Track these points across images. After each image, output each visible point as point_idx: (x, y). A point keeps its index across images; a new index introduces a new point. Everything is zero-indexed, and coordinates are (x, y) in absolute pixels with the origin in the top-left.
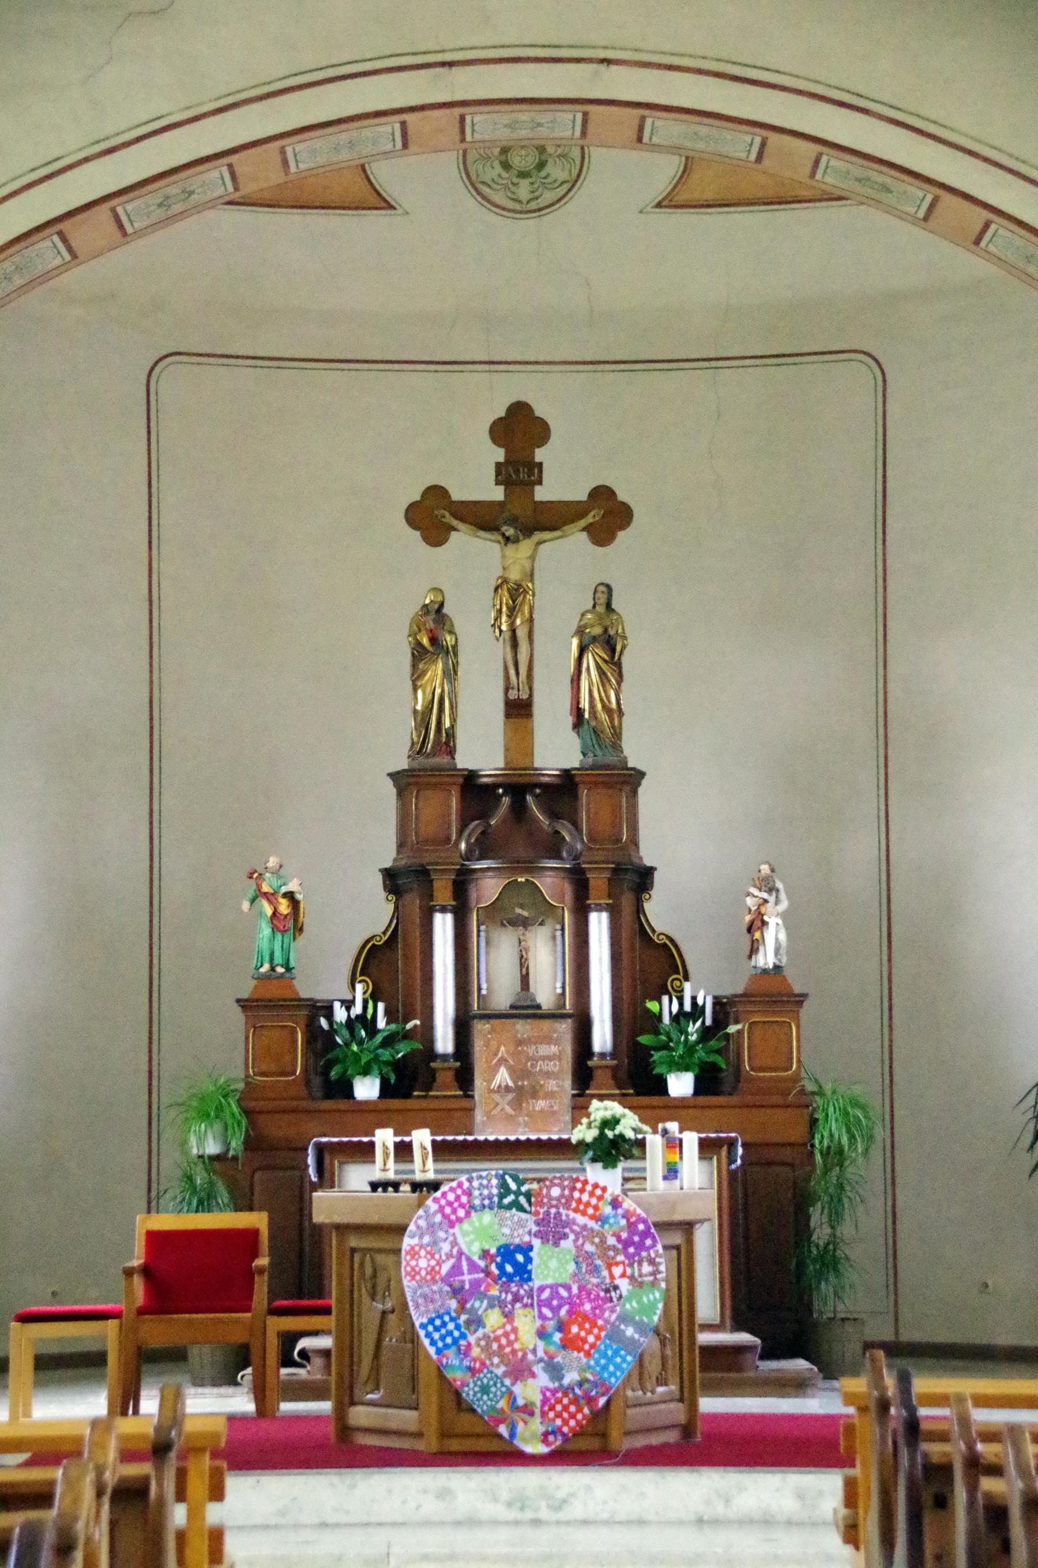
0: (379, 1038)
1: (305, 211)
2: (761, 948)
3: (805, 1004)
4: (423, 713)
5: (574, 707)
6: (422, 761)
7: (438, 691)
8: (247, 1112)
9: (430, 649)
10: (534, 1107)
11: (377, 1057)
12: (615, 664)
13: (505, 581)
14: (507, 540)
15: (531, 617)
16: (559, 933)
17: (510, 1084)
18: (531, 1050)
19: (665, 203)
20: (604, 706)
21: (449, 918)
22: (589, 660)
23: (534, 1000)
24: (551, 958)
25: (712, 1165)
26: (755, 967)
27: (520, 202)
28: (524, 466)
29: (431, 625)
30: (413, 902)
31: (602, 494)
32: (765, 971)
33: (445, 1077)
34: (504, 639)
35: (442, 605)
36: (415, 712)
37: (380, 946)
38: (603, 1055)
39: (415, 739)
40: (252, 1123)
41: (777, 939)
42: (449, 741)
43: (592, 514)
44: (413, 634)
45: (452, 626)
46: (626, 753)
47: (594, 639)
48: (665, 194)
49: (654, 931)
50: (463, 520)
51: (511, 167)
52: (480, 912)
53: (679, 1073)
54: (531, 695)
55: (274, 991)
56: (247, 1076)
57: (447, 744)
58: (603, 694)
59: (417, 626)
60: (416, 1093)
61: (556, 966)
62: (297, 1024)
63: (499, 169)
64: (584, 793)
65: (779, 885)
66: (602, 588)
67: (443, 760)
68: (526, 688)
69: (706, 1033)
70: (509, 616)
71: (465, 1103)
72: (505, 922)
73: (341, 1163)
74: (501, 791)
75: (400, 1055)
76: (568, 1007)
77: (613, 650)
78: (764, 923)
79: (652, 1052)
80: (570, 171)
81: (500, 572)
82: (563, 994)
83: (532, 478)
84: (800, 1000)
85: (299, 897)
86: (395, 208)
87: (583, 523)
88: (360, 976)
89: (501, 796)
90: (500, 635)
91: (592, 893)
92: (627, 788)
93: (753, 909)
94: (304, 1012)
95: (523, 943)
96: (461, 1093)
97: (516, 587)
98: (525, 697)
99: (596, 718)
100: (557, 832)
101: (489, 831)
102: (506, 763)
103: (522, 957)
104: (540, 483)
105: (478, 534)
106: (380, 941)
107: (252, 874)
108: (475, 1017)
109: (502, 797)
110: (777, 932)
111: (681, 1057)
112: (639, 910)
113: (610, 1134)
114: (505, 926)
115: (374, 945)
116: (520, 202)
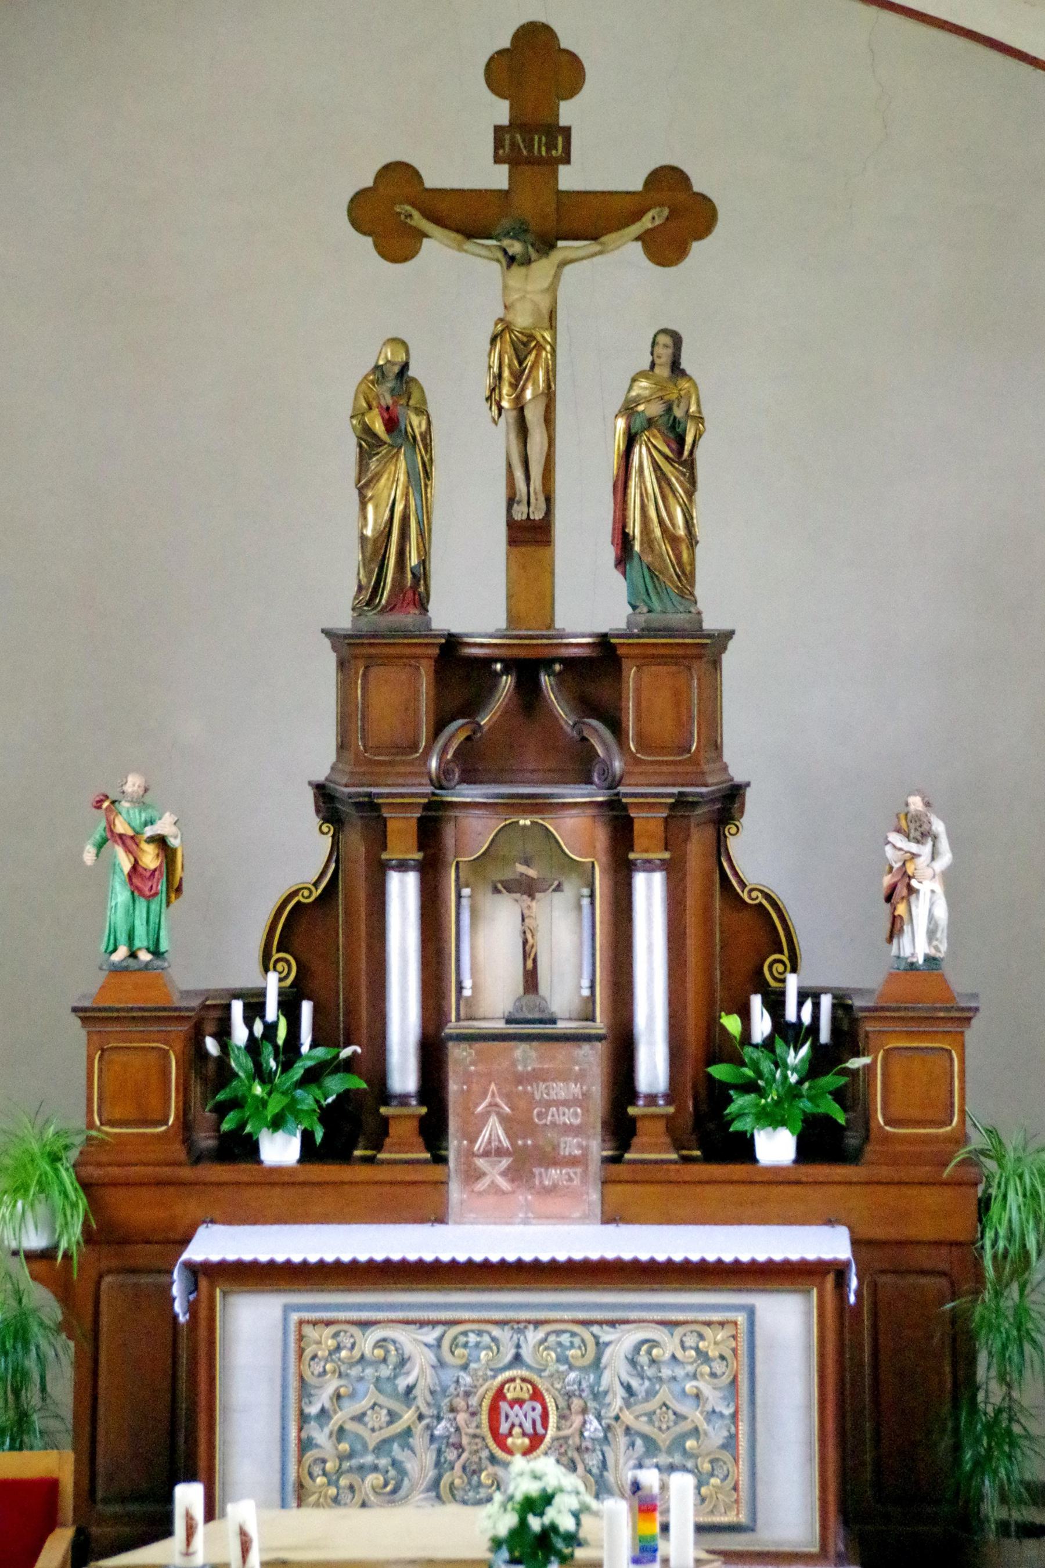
0: (298, 1072)
2: (907, 928)
3: (973, 1022)
4: (375, 540)
5: (619, 532)
6: (373, 619)
7: (399, 508)
8: (86, 1186)
11: (294, 1101)
12: (683, 463)
14: (511, 260)
15: (549, 387)
16: (586, 902)
17: (506, 1143)
18: (539, 1090)
21: (412, 879)
22: (640, 454)
25: (810, 1301)
30: (355, 841)
35: (405, 367)
36: (363, 538)
37: (309, 904)
38: (652, 1099)
39: (364, 581)
40: (95, 1204)
41: (931, 917)
43: (649, 215)
44: (357, 414)
45: (424, 401)
47: (650, 423)
49: (743, 885)
50: (438, 221)
62: (171, 1047)
64: (631, 674)
65: (938, 826)
66: (663, 339)
67: (408, 618)
70: (514, 386)
71: (434, 1172)
72: (499, 886)
73: (225, 1294)
74: (499, 666)
75: (330, 1100)
77: (681, 440)
79: (732, 1092)
81: (500, 312)
83: (554, 152)
84: (964, 1017)
85: (174, 842)
87: (636, 229)
88: (278, 951)
89: (498, 675)
90: (500, 414)
91: (638, 842)
92: (699, 668)
93: (896, 866)
94: (185, 1028)
95: (526, 920)
97: (525, 339)
98: (538, 515)
100: (584, 739)
103: (525, 942)
104: (567, 160)
105: (466, 247)
106: (309, 897)
108: (451, 1038)
110: (932, 904)
112: (720, 847)
113: (535, 1524)
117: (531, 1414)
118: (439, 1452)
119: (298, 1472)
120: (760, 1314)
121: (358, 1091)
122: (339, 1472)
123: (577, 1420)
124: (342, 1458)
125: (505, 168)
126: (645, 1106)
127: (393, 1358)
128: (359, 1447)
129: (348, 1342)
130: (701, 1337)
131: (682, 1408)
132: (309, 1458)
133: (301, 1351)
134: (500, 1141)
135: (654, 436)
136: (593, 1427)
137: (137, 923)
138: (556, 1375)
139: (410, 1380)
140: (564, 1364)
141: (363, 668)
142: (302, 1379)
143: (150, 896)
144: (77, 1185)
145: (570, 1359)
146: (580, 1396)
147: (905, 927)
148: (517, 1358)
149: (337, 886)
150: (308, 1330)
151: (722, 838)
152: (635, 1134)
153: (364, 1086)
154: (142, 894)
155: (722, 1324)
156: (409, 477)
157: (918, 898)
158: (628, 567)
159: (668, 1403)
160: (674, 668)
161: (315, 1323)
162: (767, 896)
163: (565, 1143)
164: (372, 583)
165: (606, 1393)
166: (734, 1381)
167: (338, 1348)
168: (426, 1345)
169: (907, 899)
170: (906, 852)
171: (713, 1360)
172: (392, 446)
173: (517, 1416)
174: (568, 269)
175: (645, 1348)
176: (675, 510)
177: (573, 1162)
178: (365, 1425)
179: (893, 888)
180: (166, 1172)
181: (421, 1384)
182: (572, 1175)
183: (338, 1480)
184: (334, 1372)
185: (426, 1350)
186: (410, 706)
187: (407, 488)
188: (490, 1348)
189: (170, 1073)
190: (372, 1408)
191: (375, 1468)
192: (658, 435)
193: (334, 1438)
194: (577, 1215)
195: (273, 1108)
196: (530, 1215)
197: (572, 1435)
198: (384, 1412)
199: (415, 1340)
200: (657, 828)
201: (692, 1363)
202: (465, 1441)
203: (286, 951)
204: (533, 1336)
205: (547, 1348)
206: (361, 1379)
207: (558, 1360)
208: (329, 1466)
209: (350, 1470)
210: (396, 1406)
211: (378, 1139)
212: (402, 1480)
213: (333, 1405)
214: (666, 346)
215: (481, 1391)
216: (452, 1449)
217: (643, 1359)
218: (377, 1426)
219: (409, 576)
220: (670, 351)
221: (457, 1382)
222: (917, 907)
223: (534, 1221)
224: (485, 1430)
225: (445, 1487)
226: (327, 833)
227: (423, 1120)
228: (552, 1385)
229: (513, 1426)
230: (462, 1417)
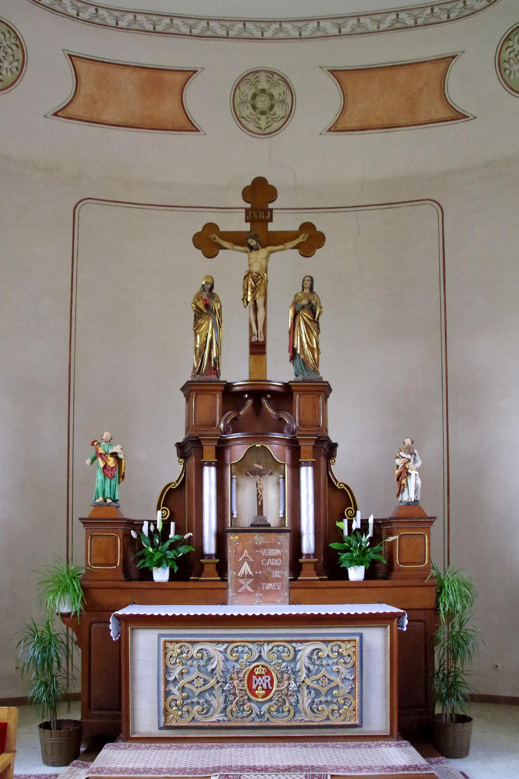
1: (155, 131)
2: (406, 489)
3: (434, 523)
7: (209, 336)
8: (84, 588)
9: (205, 311)
10: (265, 587)
11: (166, 555)
12: (315, 322)
13: (250, 272)
16: (281, 480)
17: (251, 573)
18: (264, 552)
19: (332, 129)
20: (309, 346)
21: (213, 469)
23: (265, 521)
24: (277, 496)
26: (401, 501)
27: (261, 129)
28: (262, 211)
29: (205, 297)
31: (307, 227)
32: (408, 504)
33: (210, 568)
34: (250, 307)
35: (212, 287)
36: (196, 349)
38: (308, 556)
39: (196, 366)
41: (416, 484)
43: (301, 237)
46: (321, 375)
47: (303, 307)
48: (332, 124)
49: (337, 482)
51: (257, 108)
52: (233, 467)
53: (357, 566)
54: (265, 340)
55: (102, 513)
56: (87, 565)
57: (215, 369)
58: (308, 339)
59: (198, 297)
60: (191, 578)
61: (279, 501)
63: (251, 110)
65: (416, 452)
66: (309, 278)
67: (213, 377)
68: (262, 335)
69: (374, 541)
71: (222, 585)
72: (248, 472)
74: (246, 396)
75: (180, 555)
76: (287, 526)
77: (314, 314)
78: (409, 474)
80: (286, 111)
81: (247, 268)
82: (284, 517)
83: (267, 217)
85: (121, 456)
86: (200, 131)
88: (163, 507)
89: (246, 399)
90: (247, 305)
91: (302, 454)
93: (401, 466)
95: (259, 486)
96: (220, 578)
97: (256, 275)
99: (304, 353)
100: (281, 419)
101: (239, 418)
103: (258, 494)
104: (271, 220)
107: (94, 442)
108: (229, 531)
109: (247, 400)
111: (358, 556)
112: (328, 468)
114: (248, 475)
115: (171, 488)
116: (260, 128)
117: (266, 681)
118: (226, 696)
119: (165, 705)
120: (365, 637)
121: (191, 551)
122: (183, 705)
123: (286, 683)
124: (184, 699)
125: (249, 224)
126: (305, 558)
127: (205, 657)
128: (191, 695)
129: (186, 650)
130: (340, 647)
131: (331, 677)
132: (169, 700)
133: (166, 654)
134: (248, 572)
135: (304, 312)
136: (293, 685)
137: (106, 488)
138: (277, 664)
139: (213, 666)
140: (280, 659)
142: (166, 666)
143: (111, 477)
144: (80, 588)
145: (283, 657)
146: (288, 673)
147: (405, 489)
148: (260, 657)
149: (185, 481)
150: (168, 645)
151: (329, 464)
152: (302, 570)
153: (194, 550)
154: (108, 477)
155: (349, 641)
156: (213, 325)
157: (410, 477)
159: (325, 675)
161: (171, 642)
162: (346, 486)
163: (275, 573)
164: (199, 365)
165: (299, 671)
166: (354, 665)
167: (182, 653)
168: (220, 651)
169: (406, 477)
170: (407, 459)
171: (345, 656)
172: (207, 314)
173: (260, 681)
174: (272, 255)
175: (316, 652)
177: (277, 580)
178: (194, 685)
179: (400, 474)
180: (116, 584)
181: (218, 668)
182: (277, 586)
183: (182, 708)
184: (180, 663)
185: (219, 653)
186: (212, 410)
187: (212, 329)
188: (248, 653)
189: (118, 545)
190: (197, 678)
191: (198, 703)
193: (180, 691)
194: (279, 601)
195: (157, 557)
196: (261, 601)
197: (284, 689)
198: (202, 680)
199: (215, 650)
200: (310, 449)
201: (336, 658)
202: (237, 692)
203: (165, 506)
204: (267, 648)
205: (273, 653)
206: (192, 666)
207: (278, 658)
208: (178, 702)
209: (187, 704)
210: (207, 677)
211: (201, 571)
212: (210, 708)
213: (180, 677)
214: (308, 280)
215: (244, 671)
216: (232, 695)
217: (315, 657)
218: (199, 686)
219: (213, 362)
220: (310, 283)
221: (234, 667)
222: (410, 481)
223: (262, 604)
224: (246, 687)
225: (228, 711)
226: (181, 462)
227: (218, 564)
228: (275, 669)
229: (258, 685)
230: (236, 682)
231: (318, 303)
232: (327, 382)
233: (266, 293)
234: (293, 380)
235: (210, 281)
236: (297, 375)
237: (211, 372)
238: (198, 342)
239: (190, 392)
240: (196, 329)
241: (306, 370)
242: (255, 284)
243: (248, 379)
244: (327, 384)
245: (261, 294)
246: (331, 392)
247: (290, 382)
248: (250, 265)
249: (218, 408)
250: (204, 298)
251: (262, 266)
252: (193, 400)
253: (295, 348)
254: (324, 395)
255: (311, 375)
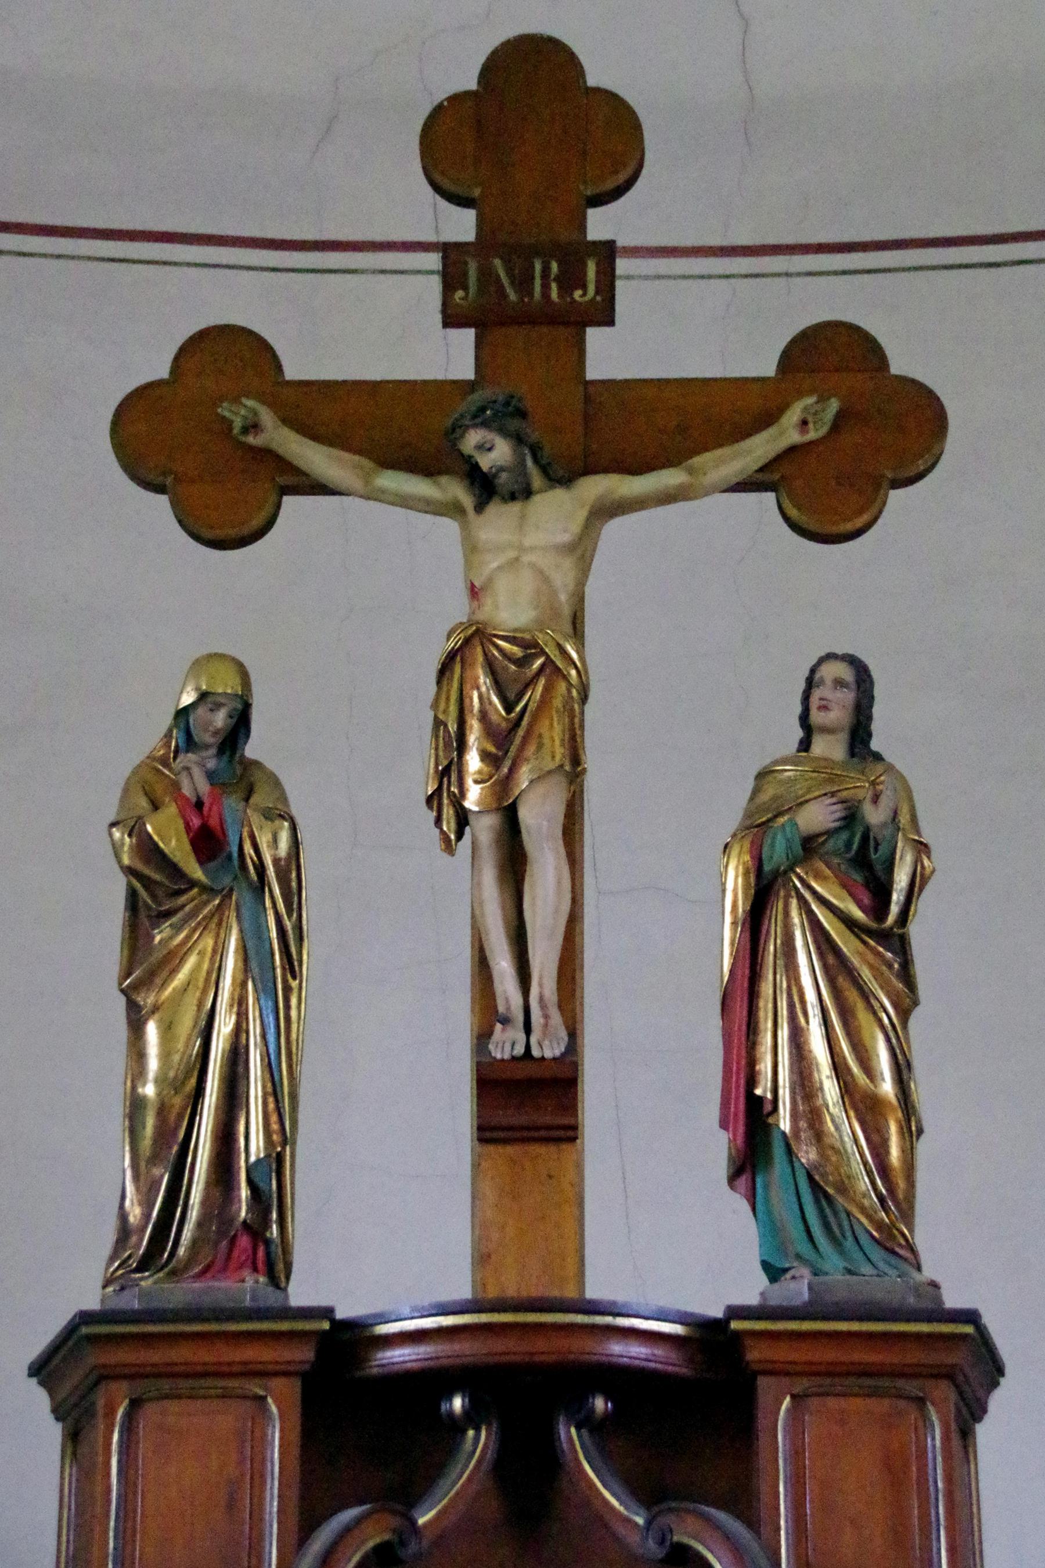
9: (197, 873)
12: (884, 937)
36: (136, 1105)
39: (135, 1213)
42: (266, 1223)
43: (793, 415)
46: (929, 1271)
57: (256, 1230)
66: (841, 670)
74: (458, 1403)
83: (577, 294)
89: (456, 1427)
97: (515, 650)
99: (819, 1135)
102: (479, 1284)
104: (609, 320)
109: (464, 1432)
125: (469, 335)
135: (818, 876)
141: (126, 1402)
156: (246, 960)
158: (759, 1181)
160: (881, 1406)
172: (208, 890)
174: (614, 529)
176: (874, 1038)
187: (244, 985)
192: (828, 872)
214: (839, 683)
219: (244, 1192)
220: (847, 697)
231: (904, 819)
232: (971, 1317)
233: (576, 759)
234: (752, 1299)
235: (227, 684)
236: (774, 1273)
237: (229, 1257)
238: (153, 1064)
239: (97, 1383)
240: (135, 987)
241: (836, 1242)
242: (509, 708)
243: (464, 1292)
244: (969, 1329)
245: (552, 766)
246: (995, 1384)
247: (735, 1312)
248: (474, 592)
249: (273, 1487)
250: (187, 791)
251: (553, 593)
252: (116, 1437)
253: (761, 1099)
254: (953, 1396)
255: (867, 1269)
